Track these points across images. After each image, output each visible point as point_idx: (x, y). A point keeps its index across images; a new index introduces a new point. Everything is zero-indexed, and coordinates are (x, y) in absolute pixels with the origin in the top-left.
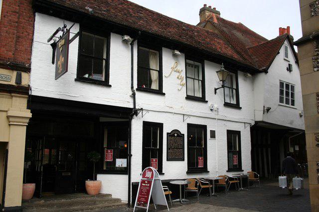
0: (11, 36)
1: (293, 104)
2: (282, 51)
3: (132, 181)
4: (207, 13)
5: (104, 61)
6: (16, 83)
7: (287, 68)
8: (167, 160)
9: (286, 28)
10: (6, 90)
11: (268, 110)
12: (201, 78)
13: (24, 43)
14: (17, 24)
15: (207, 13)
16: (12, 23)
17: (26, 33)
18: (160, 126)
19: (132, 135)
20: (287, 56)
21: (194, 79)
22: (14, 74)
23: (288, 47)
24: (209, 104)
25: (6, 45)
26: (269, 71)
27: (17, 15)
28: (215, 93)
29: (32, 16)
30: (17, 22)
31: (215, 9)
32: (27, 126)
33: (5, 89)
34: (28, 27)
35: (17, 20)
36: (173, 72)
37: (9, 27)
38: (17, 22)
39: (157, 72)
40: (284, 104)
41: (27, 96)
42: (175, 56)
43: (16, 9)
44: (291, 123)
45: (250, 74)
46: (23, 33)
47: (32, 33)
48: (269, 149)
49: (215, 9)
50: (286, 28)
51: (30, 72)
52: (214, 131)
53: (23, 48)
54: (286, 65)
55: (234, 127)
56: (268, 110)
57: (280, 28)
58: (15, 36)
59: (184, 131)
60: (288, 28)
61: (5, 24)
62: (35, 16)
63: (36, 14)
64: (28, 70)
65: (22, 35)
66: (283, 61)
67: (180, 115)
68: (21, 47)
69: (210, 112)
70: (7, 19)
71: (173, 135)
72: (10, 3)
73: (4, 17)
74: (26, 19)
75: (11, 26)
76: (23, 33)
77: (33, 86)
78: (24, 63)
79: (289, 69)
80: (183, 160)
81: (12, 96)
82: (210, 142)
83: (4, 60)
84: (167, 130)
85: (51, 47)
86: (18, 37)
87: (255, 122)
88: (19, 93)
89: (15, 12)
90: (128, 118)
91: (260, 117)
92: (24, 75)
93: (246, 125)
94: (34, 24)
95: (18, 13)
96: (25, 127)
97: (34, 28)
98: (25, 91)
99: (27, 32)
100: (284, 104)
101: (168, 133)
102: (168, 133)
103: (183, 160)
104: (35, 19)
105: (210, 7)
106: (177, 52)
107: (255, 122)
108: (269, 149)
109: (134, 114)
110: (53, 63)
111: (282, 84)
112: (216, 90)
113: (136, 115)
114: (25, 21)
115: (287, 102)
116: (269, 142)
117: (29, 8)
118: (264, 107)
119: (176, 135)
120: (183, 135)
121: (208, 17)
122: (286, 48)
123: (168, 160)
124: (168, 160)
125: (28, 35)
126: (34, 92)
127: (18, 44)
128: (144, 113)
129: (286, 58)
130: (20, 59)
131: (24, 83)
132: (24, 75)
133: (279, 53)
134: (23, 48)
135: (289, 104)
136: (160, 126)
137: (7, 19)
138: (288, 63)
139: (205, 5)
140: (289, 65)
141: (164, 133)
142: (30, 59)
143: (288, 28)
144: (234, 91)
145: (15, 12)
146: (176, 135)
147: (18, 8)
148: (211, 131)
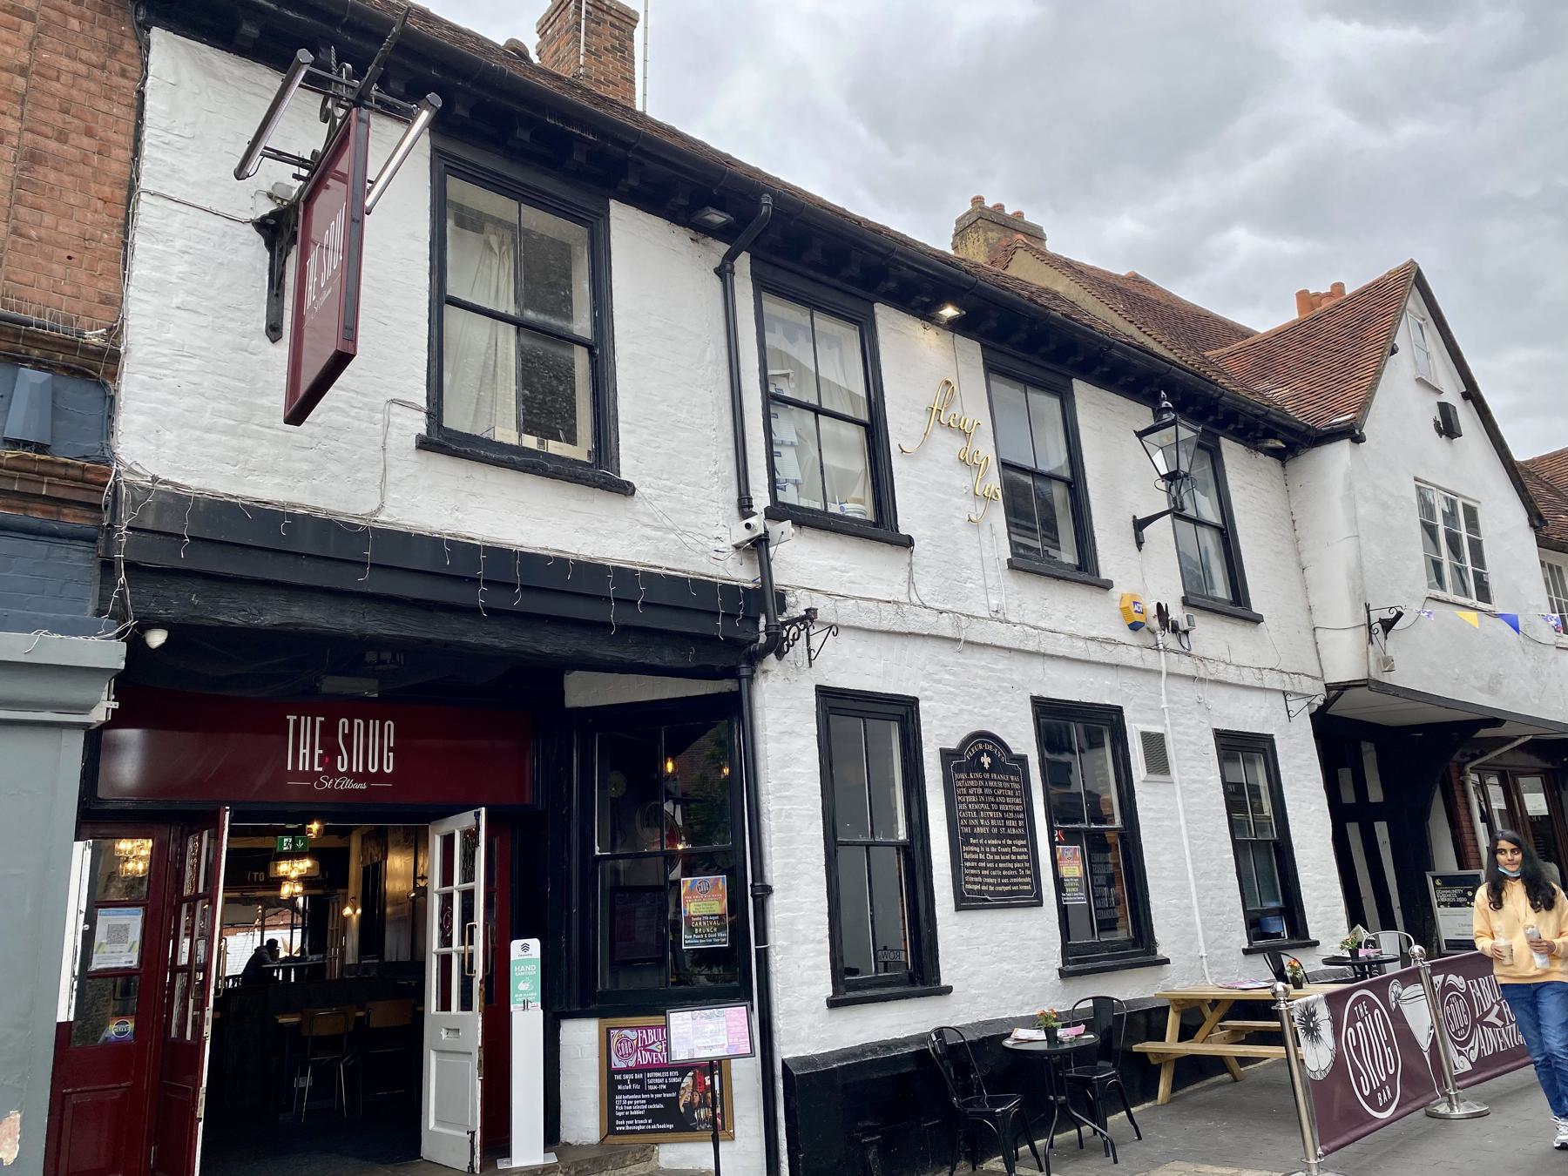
3: (786, 1050)
5: (581, 358)
7: (1437, 424)
8: (958, 908)
14: (20, 82)
17: (86, 142)
18: (904, 711)
19: (761, 765)
24: (1117, 591)
27: (27, 28)
29: (130, 46)
30: (23, 71)
34: (102, 105)
35: (24, 58)
36: (939, 435)
38: (23, 71)
44: (1491, 690)
48: (1381, 830)
52: (1161, 737)
55: (1248, 716)
59: (1022, 739)
62: (145, 47)
65: (53, 145)
68: (48, 219)
69: (1126, 636)
76: (62, 137)
78: (68, 321)
85: (257, 240)
90: (731, 673)
91: (1345, 661)
93: (1295, 705)
95: (30, 17)
99: (89, 133)
101: (946, 755)
102: (946, 755)
104: (145, 65)
108: (1381, 830)
109: (767, 650)
110: (274, 331)
112: (1140, 525)
113: (780, 655)
116: (1376, 794)
120: (1022, 760)
123: (963, 902)
124: (963, 902)
127: (29, 197)
128: (816, 642)
136: (904, 711)
138: (1433, 400)
139: (978, 201)
140: (1445, 409)
141: (925, 751)
142: (114, 302)
146: (986, 760)
148: (471, 1010)
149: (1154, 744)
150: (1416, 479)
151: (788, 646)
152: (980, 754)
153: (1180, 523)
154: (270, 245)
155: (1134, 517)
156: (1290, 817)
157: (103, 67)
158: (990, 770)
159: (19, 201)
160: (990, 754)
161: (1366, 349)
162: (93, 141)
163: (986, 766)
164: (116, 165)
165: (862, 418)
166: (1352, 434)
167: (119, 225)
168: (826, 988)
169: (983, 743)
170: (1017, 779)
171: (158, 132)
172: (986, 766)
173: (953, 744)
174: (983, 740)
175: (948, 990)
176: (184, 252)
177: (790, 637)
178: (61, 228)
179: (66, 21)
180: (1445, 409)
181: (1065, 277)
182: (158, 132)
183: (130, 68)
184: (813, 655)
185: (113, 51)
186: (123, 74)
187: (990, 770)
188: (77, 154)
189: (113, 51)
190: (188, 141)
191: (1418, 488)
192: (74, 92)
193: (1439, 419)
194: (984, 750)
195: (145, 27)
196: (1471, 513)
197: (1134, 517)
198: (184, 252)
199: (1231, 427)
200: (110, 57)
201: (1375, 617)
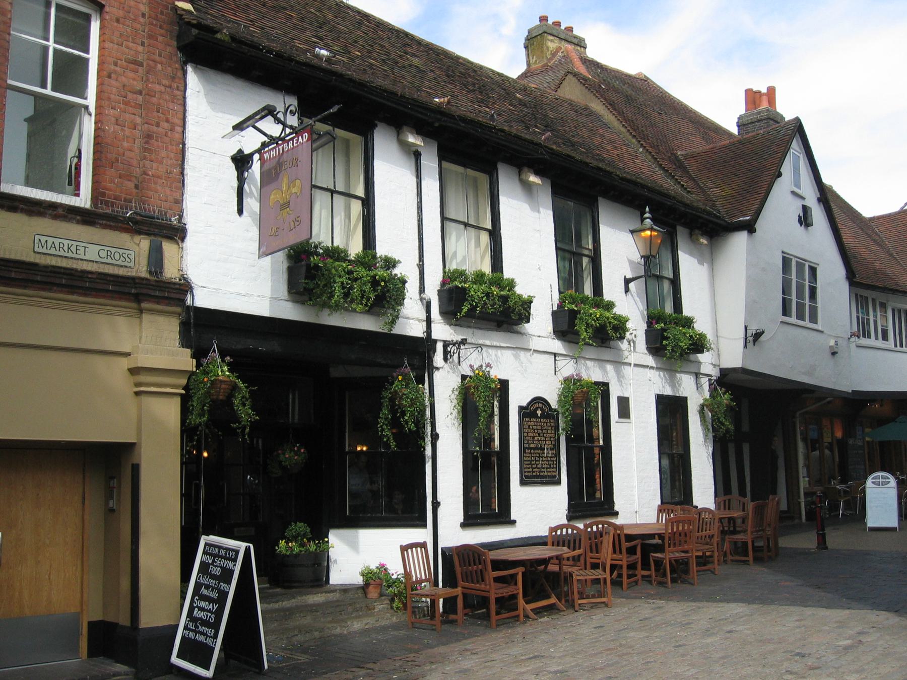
0: (127, 131)
1: (814, 319)
2: (787, 168)
3: (441, 545)
4: (552, 44)
6: (151, 273)
7: (800, 217)
9: (764, 91)
10: (129, 294)
11: (757, 336)
12: (360, 191)
13: (163, 153)
15: (550, 44)
16: (129, 94)
20: (797, 184)
21: (333, 192)
22: (144, 244)
23: (801, 156)
25: (117, 160)
26: (757, 226)
28: (627, 290)
29: (180, 74)
31: (570, 29)
32: (181, 395)
33: (127, 290)
34: (171, 106)
37: (122, 106)
39: (360, 202)
40: (806, 323)
41: (179, 309)
42: (528, 187)
43: (137, 52)
45: (537, 173)
46: (158, 125)
47: (180, 122)
49: (570, 29)
50: (764, 91)
51: (183, 239)
53: (162, 170)
54: (796, 210)
56: (757, 336)
57: (749, 92)
58: (137, 133)
59: (861, 337)
60: (771, 91)
61: (112, 96)
62: (185, 73)
63: (190, 69)
64: (178, 233)
65: (155, 128)
66: (790, 197)
67: (547, 356)
70: (118, 84)
71: (533, 414)
72: (121, 35)
73: (109, 77)
74: (165, 82)
75: (126, 103)
76: (158, 125)
77: (195, 275)
79: (805, 220)
80: (558, 482)
81: (141, 311)
82: (617, 427)
83: (113, 204)
84: (518, 398)
86: (148, 137)
87: (722, 370)
88: (158, 300)
89: (135, 62)
92: (168, 248)
94: (185, 98)
95: (141, 65)
96: (177, 401)
97: (185, 111)
98: (178, 296)
99: (167, 121)
100: (793, 320)
101: (521, 408)
102: (521, 408)
103: (558, 482)
105: (558, 24)
106: (533, 179)
107: (722, 370)
111: (786, 262)
112: (627, 281)
114: (163, 88)
115: (801, 316)
117: (169, 49)
118: (746, 328)
119: (539, 412)
121: (554, 54)
122: (796, 170)
123: (523, 482)
124: (523, 482)
125: (172, 130)
126: (202, 299)
129: (796, 190)
130: (155, 205)
131: (170, 272)
132: (168, 248)
133: (780, 175)
134: (162, 170)
135: (803, 319)
137: (118, 84)
139: (543, 19)
140: (805, 209)
142: (179, 202)
143: (771, 91)
144: (666, 286)
145: (135, 62)
146: (539, 412)
147: (140, 48)
149: (624, 403)
150: (783, 252)
151: (451, 356)
152: (537, 409)
153: (650, 281)
154: (237, 168)
155: (625, 277)
156: (691, 441)
157: (170, 87)
158: (540, 417)
159: (145, 158)
160: (542, 409)
161: (765, 173)
162: (168, 124)
163: (539, 415)
164: (177, 136)
165: (488, 228)
166: (750, 227)
167: (180, 164)
168: (461, 518)
169: (543, 404)
170: (553, 421)
171: (194, 117)
172: (539, 415)
173: (524, 404)
174: (539, 401)
175: (514, 522)
176: (206, 176)
177: (452, 351)
178: (159, 169)
179: (156, 65)
180: (805, 209)
181: (597, 99)
182: (194, 117)
183: (180, 85)
184: (53, 246)
185: (173, 78)
186: (178, 89)
187: (540, 417)
188: (164, 131)
189: (173, 78)
190: (204, 120)
191: (784, 257)
192: (161, 101)
193: (802, 215)
194: (539, 407)
195: (186, 63)
196: (813, 270)
197: (625, 277)
198: (206, 176)
199: (683, 221)
200: (173, 81)
201: (749, 333)
